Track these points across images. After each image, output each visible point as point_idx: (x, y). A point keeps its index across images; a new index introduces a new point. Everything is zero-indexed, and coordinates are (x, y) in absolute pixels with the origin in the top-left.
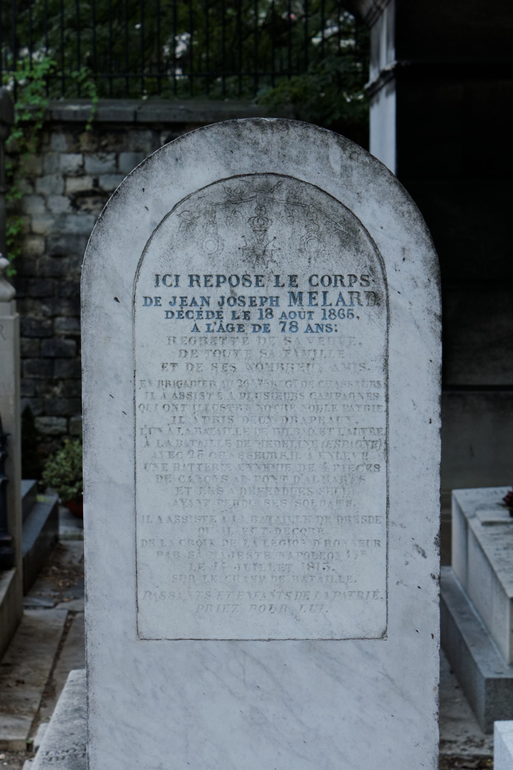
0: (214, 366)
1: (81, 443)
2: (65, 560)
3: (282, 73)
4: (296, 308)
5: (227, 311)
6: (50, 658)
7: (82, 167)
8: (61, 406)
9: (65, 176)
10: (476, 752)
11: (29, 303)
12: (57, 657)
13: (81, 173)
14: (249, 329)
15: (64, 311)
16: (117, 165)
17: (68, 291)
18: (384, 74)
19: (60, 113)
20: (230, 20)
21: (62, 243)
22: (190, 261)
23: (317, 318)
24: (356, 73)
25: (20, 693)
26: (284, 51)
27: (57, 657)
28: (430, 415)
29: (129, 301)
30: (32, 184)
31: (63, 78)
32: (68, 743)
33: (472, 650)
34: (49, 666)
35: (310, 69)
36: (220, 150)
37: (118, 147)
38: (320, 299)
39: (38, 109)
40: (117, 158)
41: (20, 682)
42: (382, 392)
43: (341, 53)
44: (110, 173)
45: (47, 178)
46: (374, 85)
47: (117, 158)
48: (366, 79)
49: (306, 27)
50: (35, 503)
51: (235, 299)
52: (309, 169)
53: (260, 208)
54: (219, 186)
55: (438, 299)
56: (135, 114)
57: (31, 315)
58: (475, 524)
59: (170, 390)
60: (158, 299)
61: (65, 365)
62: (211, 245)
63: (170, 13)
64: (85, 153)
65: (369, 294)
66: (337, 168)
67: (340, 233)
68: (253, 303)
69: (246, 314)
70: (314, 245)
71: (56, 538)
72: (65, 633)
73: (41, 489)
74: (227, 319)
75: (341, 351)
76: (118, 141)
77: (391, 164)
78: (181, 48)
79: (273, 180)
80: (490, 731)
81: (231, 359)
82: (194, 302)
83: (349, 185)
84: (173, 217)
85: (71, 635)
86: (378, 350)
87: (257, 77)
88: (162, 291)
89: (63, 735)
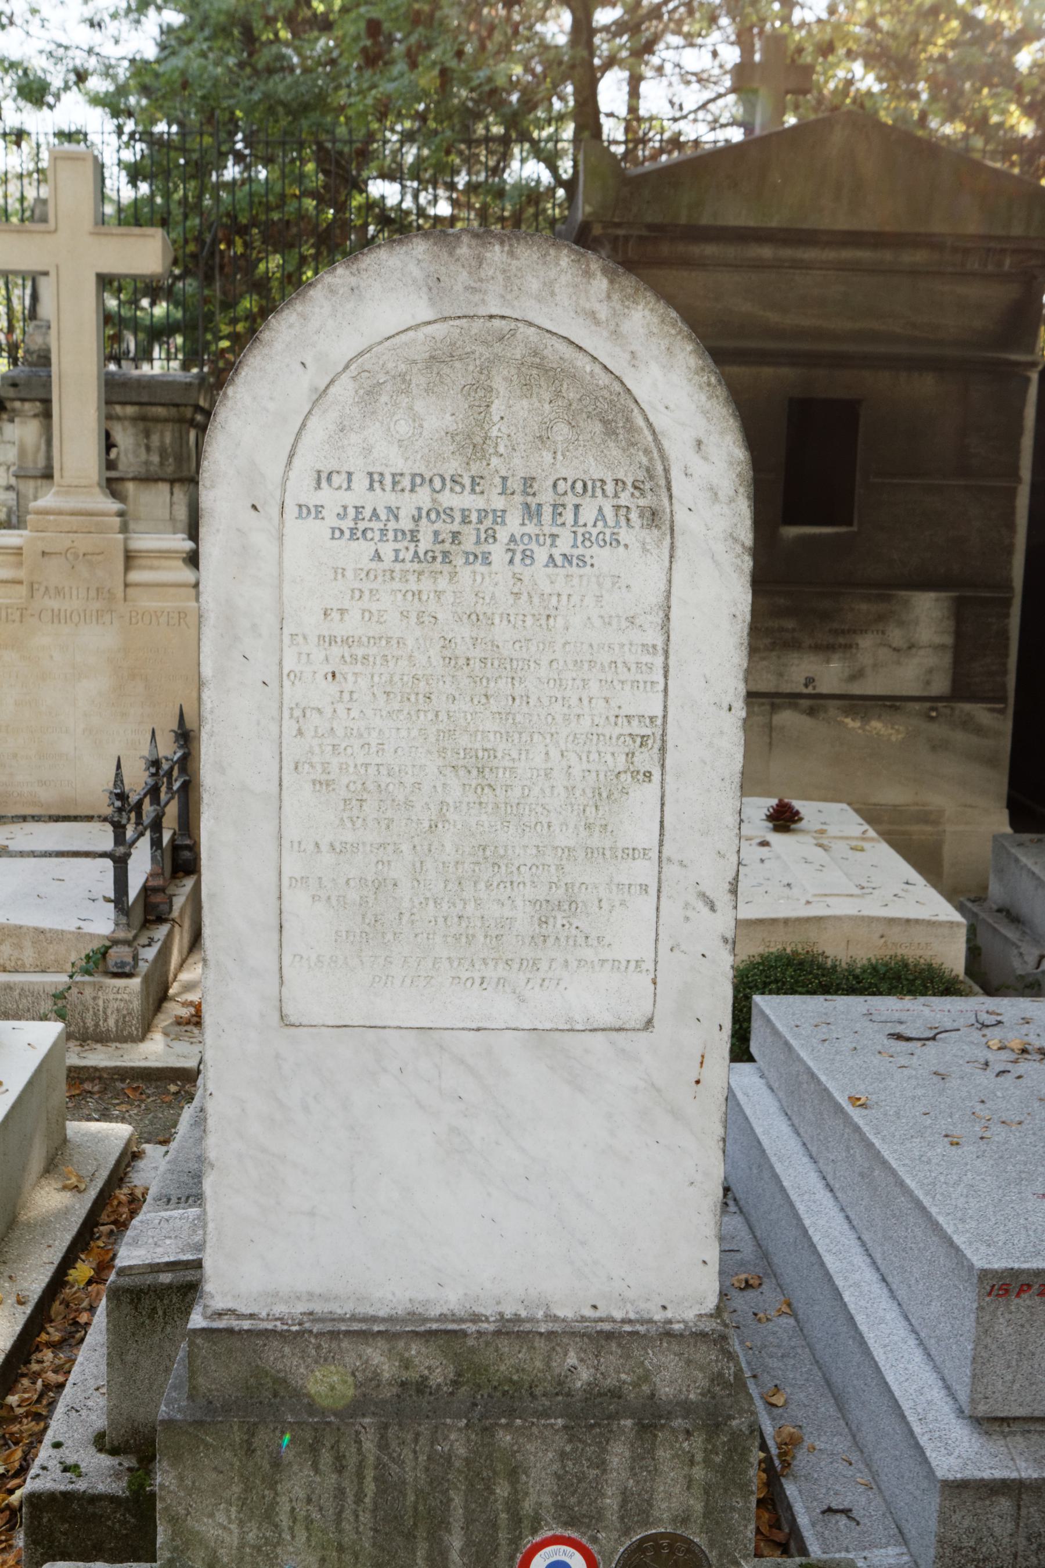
0: (404, 615)
4: (531, 528)
14: (460, 561)
22: (367, 451)
23: (564, 545)
29: (275, 511)
38: (569, 516)
42: (659, 660)
55: (748, 523)
59: (336, 651)
62: (404, 428)
68: (465, 520)
69: (455, 535)
70: (562, 432)
75: (599, 598)
81: (432, 607)
82: (375, 514)
84: (345, 378)
86: (653, 596)
88: (326, 496)
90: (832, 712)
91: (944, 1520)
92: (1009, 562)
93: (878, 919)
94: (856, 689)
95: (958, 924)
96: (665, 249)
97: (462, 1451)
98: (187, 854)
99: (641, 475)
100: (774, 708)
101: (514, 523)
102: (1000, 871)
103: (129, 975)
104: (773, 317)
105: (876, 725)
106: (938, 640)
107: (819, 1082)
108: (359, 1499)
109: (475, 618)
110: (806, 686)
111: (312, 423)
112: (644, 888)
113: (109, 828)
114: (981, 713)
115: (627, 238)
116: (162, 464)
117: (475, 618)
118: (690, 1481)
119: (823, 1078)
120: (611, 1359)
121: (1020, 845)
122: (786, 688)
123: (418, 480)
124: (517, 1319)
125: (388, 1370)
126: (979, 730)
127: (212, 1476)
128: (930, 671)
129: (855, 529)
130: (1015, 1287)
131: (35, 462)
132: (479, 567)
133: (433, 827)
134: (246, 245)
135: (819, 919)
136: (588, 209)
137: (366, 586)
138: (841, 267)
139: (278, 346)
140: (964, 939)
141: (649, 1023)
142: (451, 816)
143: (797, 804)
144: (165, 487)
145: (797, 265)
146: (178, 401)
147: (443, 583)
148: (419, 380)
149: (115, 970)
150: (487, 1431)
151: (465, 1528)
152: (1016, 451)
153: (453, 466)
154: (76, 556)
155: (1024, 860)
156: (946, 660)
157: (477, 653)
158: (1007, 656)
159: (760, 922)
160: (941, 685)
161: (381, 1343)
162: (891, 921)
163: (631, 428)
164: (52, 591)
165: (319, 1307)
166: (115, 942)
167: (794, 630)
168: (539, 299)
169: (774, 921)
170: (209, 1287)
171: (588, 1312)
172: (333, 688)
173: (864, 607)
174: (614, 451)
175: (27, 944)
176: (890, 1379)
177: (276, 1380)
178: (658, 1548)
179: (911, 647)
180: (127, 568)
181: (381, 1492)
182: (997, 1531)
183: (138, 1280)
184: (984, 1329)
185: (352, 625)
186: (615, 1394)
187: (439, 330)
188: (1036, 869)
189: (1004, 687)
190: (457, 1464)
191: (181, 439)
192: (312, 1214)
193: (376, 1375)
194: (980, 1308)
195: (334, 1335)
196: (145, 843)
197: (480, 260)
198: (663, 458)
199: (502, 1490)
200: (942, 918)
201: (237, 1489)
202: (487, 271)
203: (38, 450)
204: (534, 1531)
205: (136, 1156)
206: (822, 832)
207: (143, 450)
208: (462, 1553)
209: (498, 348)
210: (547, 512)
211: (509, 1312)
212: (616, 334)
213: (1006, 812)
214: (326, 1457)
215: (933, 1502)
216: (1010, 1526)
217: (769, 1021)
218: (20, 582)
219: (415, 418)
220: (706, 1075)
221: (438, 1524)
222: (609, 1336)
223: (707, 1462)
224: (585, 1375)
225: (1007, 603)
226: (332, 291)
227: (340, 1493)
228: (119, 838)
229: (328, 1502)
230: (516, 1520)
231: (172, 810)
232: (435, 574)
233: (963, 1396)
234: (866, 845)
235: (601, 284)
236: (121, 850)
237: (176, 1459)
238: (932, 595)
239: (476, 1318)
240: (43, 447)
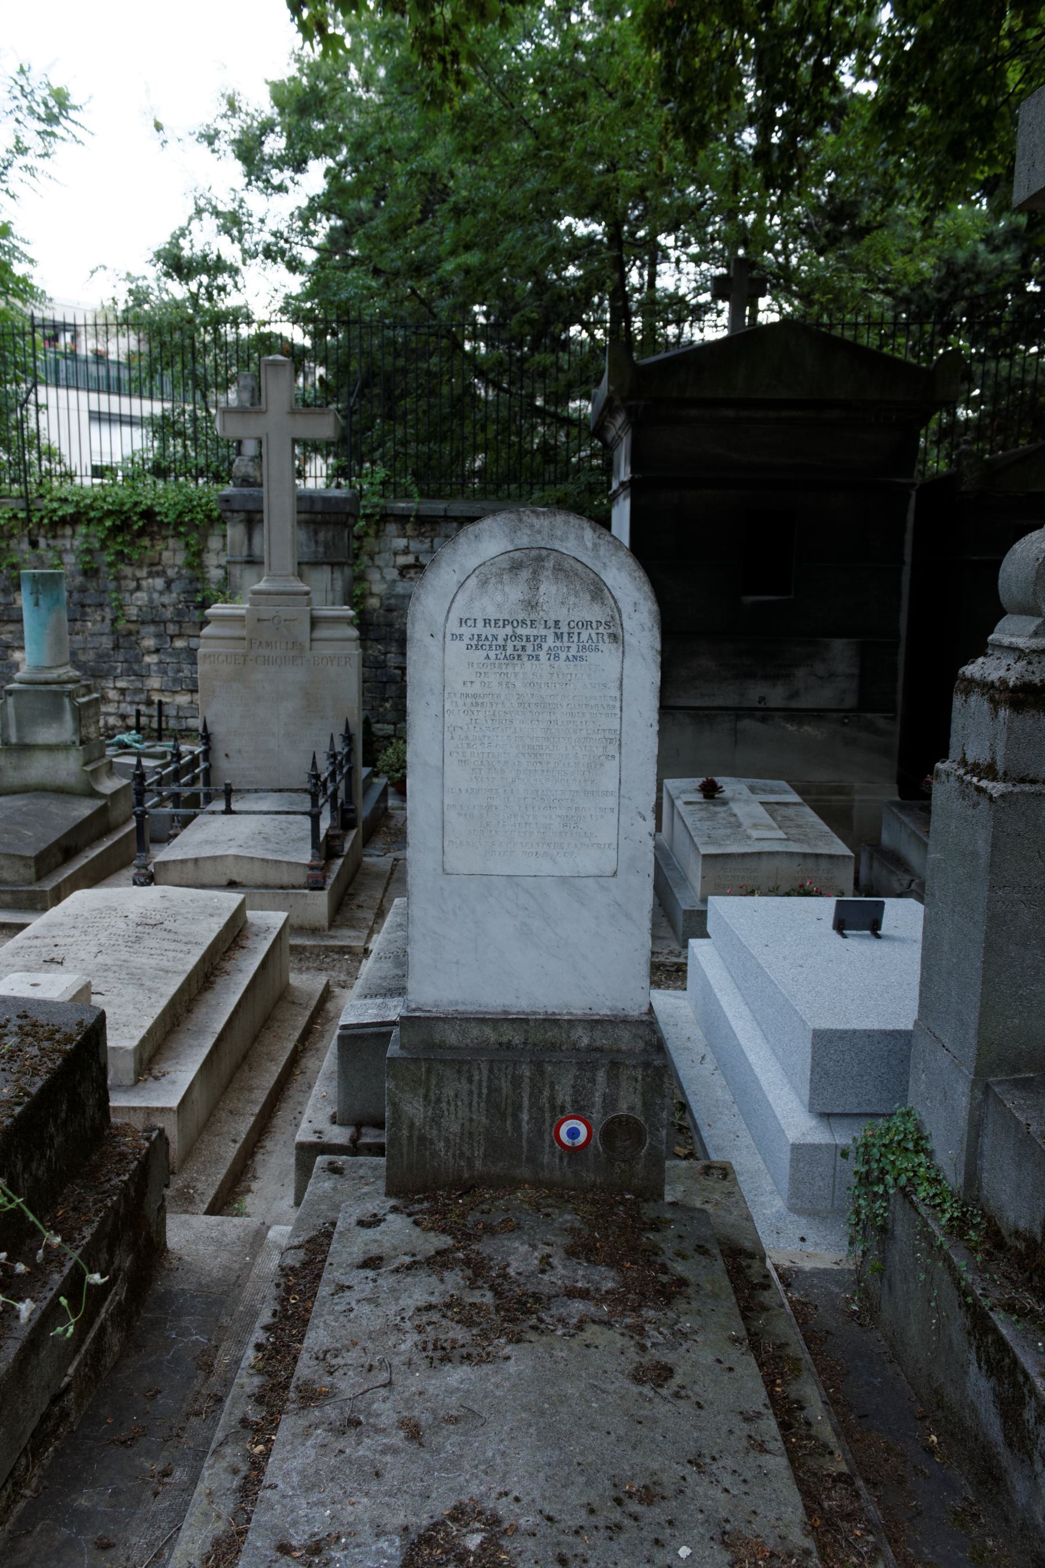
0: (500, 684)
1: (405, 742)
2: (392, 823)
3: (550, 482)
4: (558, 644)
5: (510, 645)
6: (381, 890)
7: (407, 547)
8: (390, 716)
9: (395, 554)
10: (675, 960)
11: (369, 643)
12: (386, 889)
13: (406, 552)
15: (393, 649)
16: (432, 547)
17: (396, 636)
18: (622, 484)
19: (392, 508)
20: (514, 444)
21: (392, 601)
22: (484, 609)
23: (573, 651)
24: (602, 483)
25: (360, 914)
26: (552, 467)
27: (386, 889)
29: (441, 637)
30: (372, 559)
31: (395, 484)
32: (393, 947)
33: (675, 890)
34: (379, 896)
35: (570, 480)
36: (507, 531)
38: (575, 638)
39: (376, 506)
41: (360, 907)
42: (618, 704)
43: (592, 469)
44: (427, 552)
45: (383, 555)
48: (610, 488)
49: (567, 449)
50: (372, 783)
51: (516, 636)
52: (569, 545)
53: (534, 572)
54: (506, 556)
55: (659, 639)
56: (446, 510)
57: (370, 652)
58: (679, 803)
59: (469, 701)
60: (461, 636)
61: (394, 687)
62: (499, 598)
63: (471, 439)
64: (409, 538)
65: (610, 635)
66: (590, 545)
67: (590, 591)
69: (523, 648)
70: (572, 599)
71: (386, 809)
72: (392, 874)
73: (375, 774)
74: (510, 650)
75: (589, 675)
76: (433, 530)
77: (626, 541)
78: (478, 464)
79: (544, 553)
80: (685, 946)
81: (513, 680)
82: (487, 638)
83: (597, 557)
84: (473, 577)
85: (396, 875)
87: (532, 485)
88: (464, 630)
89: (390, 942)
94: (794, 704)
95: (849, 857)
97: (528, 1074)
98: (351, 815)
100: (738, 718)
105: (807, 728)
112: (612, 810)
113: (308, 797)
114: (879, 720)
132: (534, 662)
144: (327, 569)
160: (851, 701)
165: (461, 1008)
171: (588, 1011)
178: (620, 1122)
181: (489, 1094)
185: (476, 688)
192: (457, 963)
196: (327, 807)
199: (546, 1093)
207: (313, 543)
208: (528, 1123)
211: (550, 1011)
213: (896, 786)
221: (519, 1108)
222: (597, 1021)
224: (585, 1041)
227: (471, 1092)
228: (314, 802)
231: (342, 786)
232: (514, 665)
236: (316, 810)
238: (845, 640)
239: (535, 1013)
240: (246, 542)
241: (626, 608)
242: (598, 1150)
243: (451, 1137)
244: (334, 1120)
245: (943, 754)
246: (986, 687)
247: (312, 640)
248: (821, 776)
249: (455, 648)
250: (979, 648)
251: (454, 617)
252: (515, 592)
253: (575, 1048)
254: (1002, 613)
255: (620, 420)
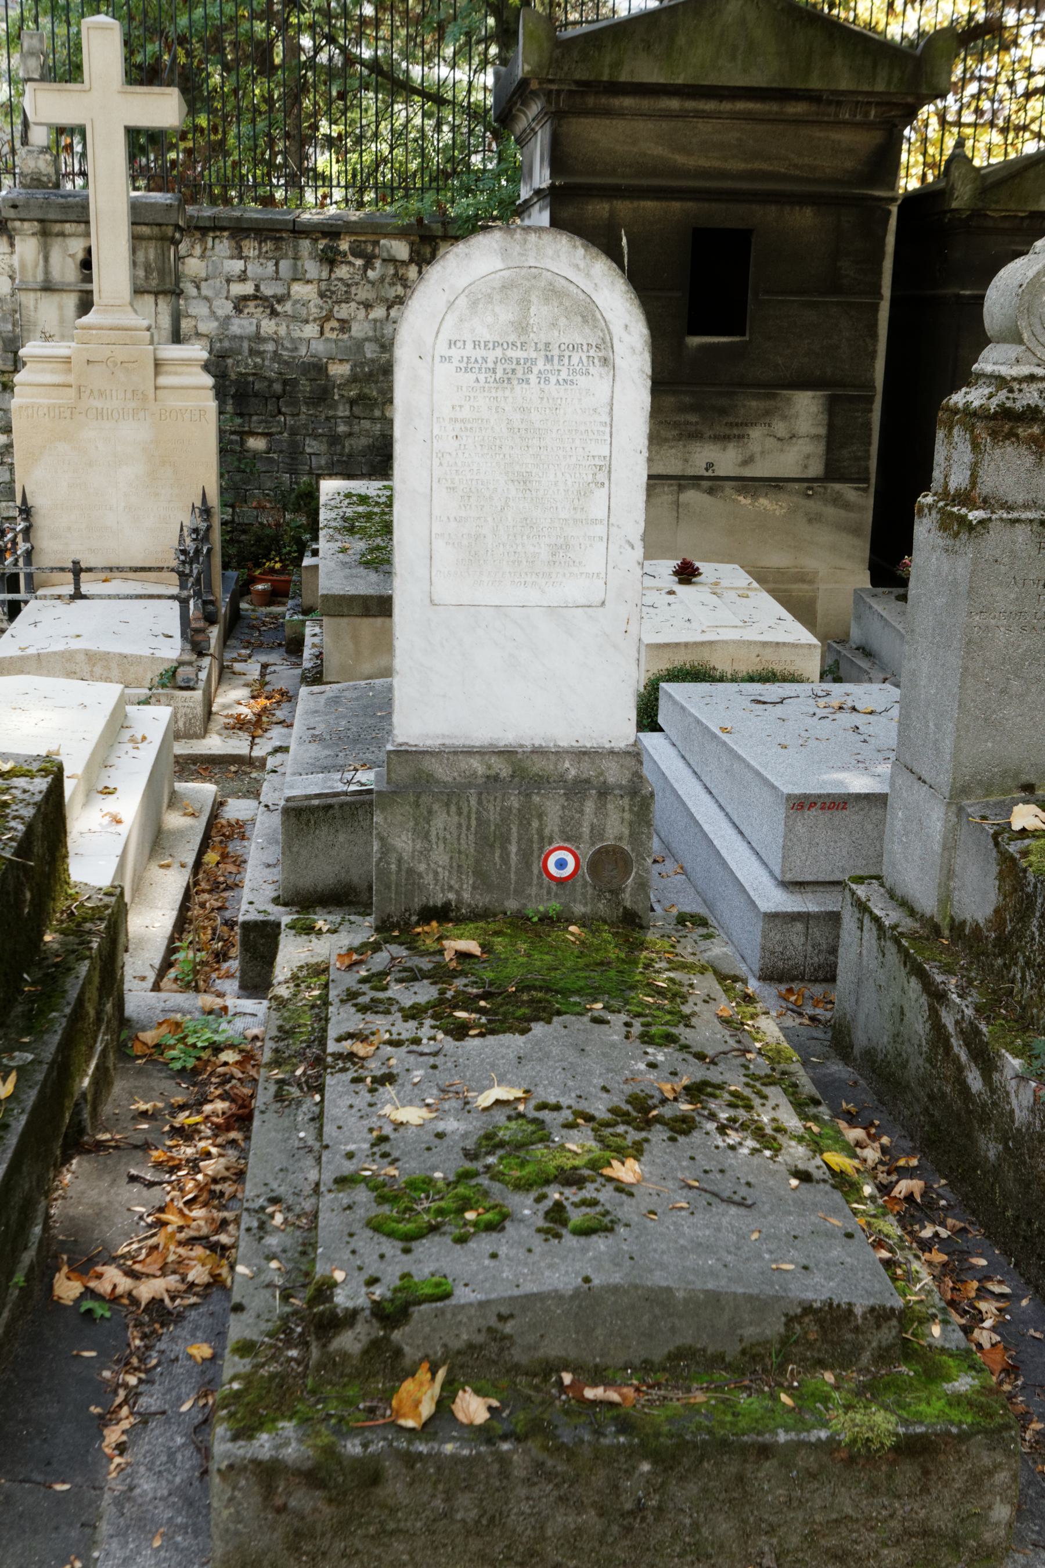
0: (490, 408)
4: (548, 367)
7: (245, 272)
13: (243, 278)
14: (515, 382)
16: (277, 272)
18: (538, 192)
22: (473, 330)
23: (564, 375)
28: (639, 448)
29: (430, 359)
37: (278, 254)
38: (566, 361)
40: (277, 264)
42: (608, 429)
46: (526, 201)
47: (277, 264)
59: (458, 425)
60: (450, 358)
62: (490, 319)
64: (246, 259)
68: (518, 363)
69: (513, 370)
70: (563, 321)
74: (500, 374)
76: (278, 249)
82: (476, 361)
86: (605, 399)
88: (453, 352)
90: (728, 491)
91: (765, 936)
92: (873, 367)
93: (755, 643)
94: (748, 472)
95: (815, 646)
96: (591, 101)
97: (517, 805)
99: (600, 341)
100: (681, 488)
101: (541, 365)
102: (859, 618)
103: (193, 689)
104: (680, 159)
105: (763, 502)
106: (814, 431)
107: (702, 724)
108: (468, 829)
109: (522, 409)
110: (707, 470)
111: (448, 317)
112: (601, 538)
114: (848, 491)
115: (559, 92)
116: (147, 278)
117: (522, 409)
118: (623, 820)
119: (704, 721)
120: (585, 764)
121: (875, 596)
122: (690, 472)
123: (496, 344)
124: (541, 746)
125: (481, 770)
126: (847, 506)
127: (399, 817)
128: (808, 457)
129: (747, 338)
130: (807, 804)
131: (35, 277)
132: (524, 385)
133: (502, 509)
134: (189, 54)
135: (711, 643)
136: (527, 68)
137: (472, 395)
138: (735, 116)
139: (432, 281)
140: (819, 658)
141: (603, 603)
142: (511, 504)
143: (697, 564)
145: (700, 114)
146: (160, 221)
147: (507, 393)
148: (497, 297)
149: (183, 684)
150: (528, 796)
151: (518, 842)
152: (879, 273)
153: (512, 338)
154: (115, 364)
155: (875, 606)
156: (820, 448)
157: (523, 426)
158: (870, 444)
159: (667, 645)
160: (816, 469)
161: (477, 757)
162: (765, 644)
163: (595, 320)
164: (96, 394)
165: (447, 742)
166: (181, 663)
167: (697, 423)
168: (552, 259)
169: (677, 645)
170: (395, 732)
171: (575, 744)
172: (456, 443)
173: (754, 404)
174: (587, 331)
175: (114, 665)
176: (738, 875)
177: (428, 775)
179: (792, 437)
180: (157, 374)
181: (478, 825)
182: (795, 942)
183: (299, 804)
184: (789, 829)
185: (466, 413)
186: (587, 781)
187: (506, 273)
188: (884, 614)
189: (867, 469)
190: (514, 811)
191: (163, 256)
193: (475, 772)
194: (787, 817)
195: (455, 753)
197: (525, 241)
198: (610, 333)
199: (535, 824)
200: (803, 641)
201: (412, 824)
202: (529, 246)
203: (36, 266)
204: (550, 844)
205: (222, 804)
206: (717, 584)
209: (533, 281)
210: (556, 359)
212: (588, 275)
213: (868, 573)
214: (453, 809)
215: (758, 928)
216: (803, 939)
217: (670, 696)
218: (70, 386)
219: (495, 315)
220: (630, 629)
221: (506, 840)
222: (585, 753)
223: (631, 810)
224: (573, 772)
225: (870, 400)
226: (457, 255)
227: (460, 825)
229: (453, 829)
230: (542, 838)
232: (504, 389)
233: (777, 872)
234: (750, 593)
235: (581, 251)
237: (383, 810)
238: (810, 394)
239: (521, 746)
240: (41, 263)
241: (617, 329)
242: (584, 879)
243: (440, 870)
244: (276, 901)
245: (925, 485)
246: (971, 415)
247: (156, 388)
248: (777, 559)
249: (443, 370)
250: (964, 378)
251: (444, 337)
252: (505, 314)
253: (562, 779)
254: (988, 341)
255: (535, 108)
